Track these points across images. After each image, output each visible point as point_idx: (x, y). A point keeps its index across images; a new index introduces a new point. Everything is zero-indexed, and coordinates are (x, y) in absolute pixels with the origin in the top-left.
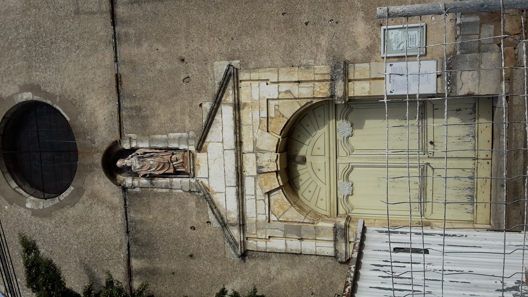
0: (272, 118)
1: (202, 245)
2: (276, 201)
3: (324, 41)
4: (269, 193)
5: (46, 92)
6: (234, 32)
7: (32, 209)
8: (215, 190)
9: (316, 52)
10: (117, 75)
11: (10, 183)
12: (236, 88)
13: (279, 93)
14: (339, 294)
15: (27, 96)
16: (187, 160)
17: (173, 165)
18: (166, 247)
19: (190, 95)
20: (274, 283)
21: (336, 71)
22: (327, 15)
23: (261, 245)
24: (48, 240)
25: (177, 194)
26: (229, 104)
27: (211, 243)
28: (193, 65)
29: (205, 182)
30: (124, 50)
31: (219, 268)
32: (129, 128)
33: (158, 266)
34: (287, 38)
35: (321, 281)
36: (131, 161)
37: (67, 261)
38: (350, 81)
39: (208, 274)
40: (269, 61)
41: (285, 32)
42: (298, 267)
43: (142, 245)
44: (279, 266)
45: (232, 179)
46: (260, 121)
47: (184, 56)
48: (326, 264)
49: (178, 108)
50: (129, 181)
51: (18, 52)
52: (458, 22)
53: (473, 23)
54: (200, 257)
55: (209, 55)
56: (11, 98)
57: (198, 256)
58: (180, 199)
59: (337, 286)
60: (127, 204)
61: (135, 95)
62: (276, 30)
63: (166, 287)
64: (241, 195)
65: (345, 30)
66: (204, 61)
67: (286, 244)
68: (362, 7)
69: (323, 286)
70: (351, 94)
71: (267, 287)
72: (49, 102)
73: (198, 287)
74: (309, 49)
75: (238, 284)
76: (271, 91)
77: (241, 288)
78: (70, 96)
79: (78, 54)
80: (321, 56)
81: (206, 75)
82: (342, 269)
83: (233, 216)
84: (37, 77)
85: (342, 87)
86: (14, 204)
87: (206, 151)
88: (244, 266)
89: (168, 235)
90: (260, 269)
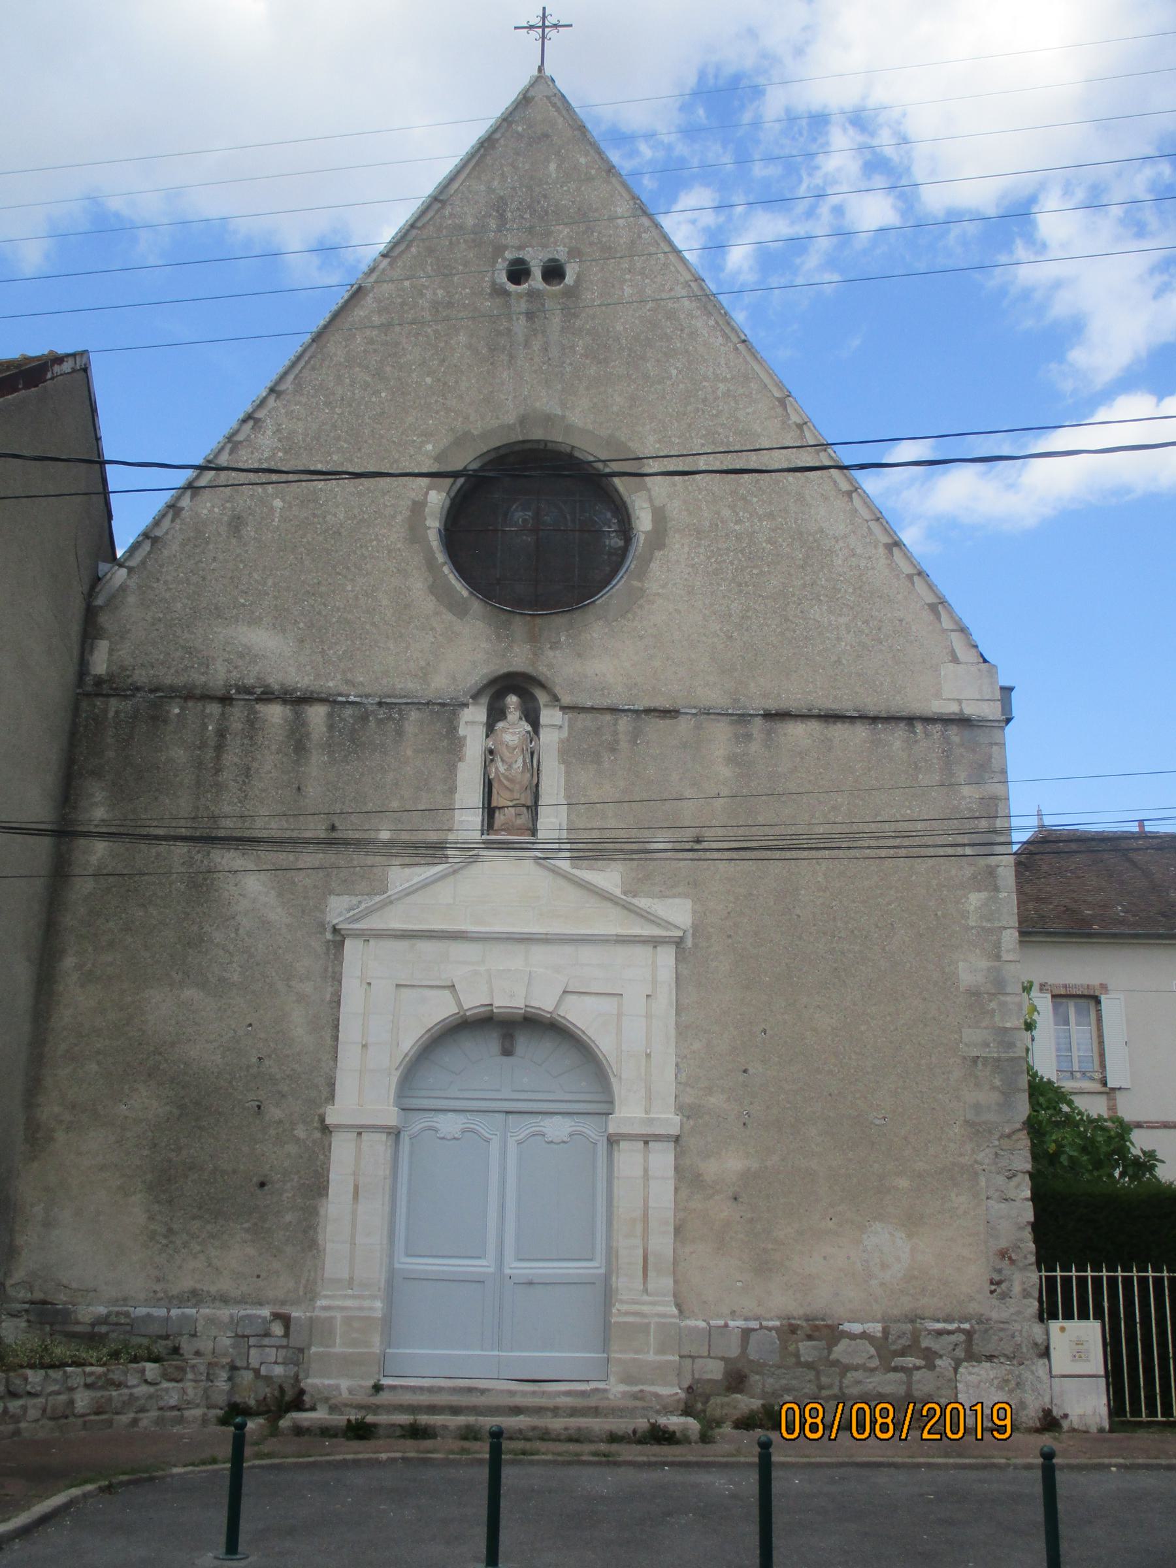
5: (650, 561)
10: (677, 712)
71: (274, 974)
75: (277, 917)
79: (718, 636)
84: (678, 547)
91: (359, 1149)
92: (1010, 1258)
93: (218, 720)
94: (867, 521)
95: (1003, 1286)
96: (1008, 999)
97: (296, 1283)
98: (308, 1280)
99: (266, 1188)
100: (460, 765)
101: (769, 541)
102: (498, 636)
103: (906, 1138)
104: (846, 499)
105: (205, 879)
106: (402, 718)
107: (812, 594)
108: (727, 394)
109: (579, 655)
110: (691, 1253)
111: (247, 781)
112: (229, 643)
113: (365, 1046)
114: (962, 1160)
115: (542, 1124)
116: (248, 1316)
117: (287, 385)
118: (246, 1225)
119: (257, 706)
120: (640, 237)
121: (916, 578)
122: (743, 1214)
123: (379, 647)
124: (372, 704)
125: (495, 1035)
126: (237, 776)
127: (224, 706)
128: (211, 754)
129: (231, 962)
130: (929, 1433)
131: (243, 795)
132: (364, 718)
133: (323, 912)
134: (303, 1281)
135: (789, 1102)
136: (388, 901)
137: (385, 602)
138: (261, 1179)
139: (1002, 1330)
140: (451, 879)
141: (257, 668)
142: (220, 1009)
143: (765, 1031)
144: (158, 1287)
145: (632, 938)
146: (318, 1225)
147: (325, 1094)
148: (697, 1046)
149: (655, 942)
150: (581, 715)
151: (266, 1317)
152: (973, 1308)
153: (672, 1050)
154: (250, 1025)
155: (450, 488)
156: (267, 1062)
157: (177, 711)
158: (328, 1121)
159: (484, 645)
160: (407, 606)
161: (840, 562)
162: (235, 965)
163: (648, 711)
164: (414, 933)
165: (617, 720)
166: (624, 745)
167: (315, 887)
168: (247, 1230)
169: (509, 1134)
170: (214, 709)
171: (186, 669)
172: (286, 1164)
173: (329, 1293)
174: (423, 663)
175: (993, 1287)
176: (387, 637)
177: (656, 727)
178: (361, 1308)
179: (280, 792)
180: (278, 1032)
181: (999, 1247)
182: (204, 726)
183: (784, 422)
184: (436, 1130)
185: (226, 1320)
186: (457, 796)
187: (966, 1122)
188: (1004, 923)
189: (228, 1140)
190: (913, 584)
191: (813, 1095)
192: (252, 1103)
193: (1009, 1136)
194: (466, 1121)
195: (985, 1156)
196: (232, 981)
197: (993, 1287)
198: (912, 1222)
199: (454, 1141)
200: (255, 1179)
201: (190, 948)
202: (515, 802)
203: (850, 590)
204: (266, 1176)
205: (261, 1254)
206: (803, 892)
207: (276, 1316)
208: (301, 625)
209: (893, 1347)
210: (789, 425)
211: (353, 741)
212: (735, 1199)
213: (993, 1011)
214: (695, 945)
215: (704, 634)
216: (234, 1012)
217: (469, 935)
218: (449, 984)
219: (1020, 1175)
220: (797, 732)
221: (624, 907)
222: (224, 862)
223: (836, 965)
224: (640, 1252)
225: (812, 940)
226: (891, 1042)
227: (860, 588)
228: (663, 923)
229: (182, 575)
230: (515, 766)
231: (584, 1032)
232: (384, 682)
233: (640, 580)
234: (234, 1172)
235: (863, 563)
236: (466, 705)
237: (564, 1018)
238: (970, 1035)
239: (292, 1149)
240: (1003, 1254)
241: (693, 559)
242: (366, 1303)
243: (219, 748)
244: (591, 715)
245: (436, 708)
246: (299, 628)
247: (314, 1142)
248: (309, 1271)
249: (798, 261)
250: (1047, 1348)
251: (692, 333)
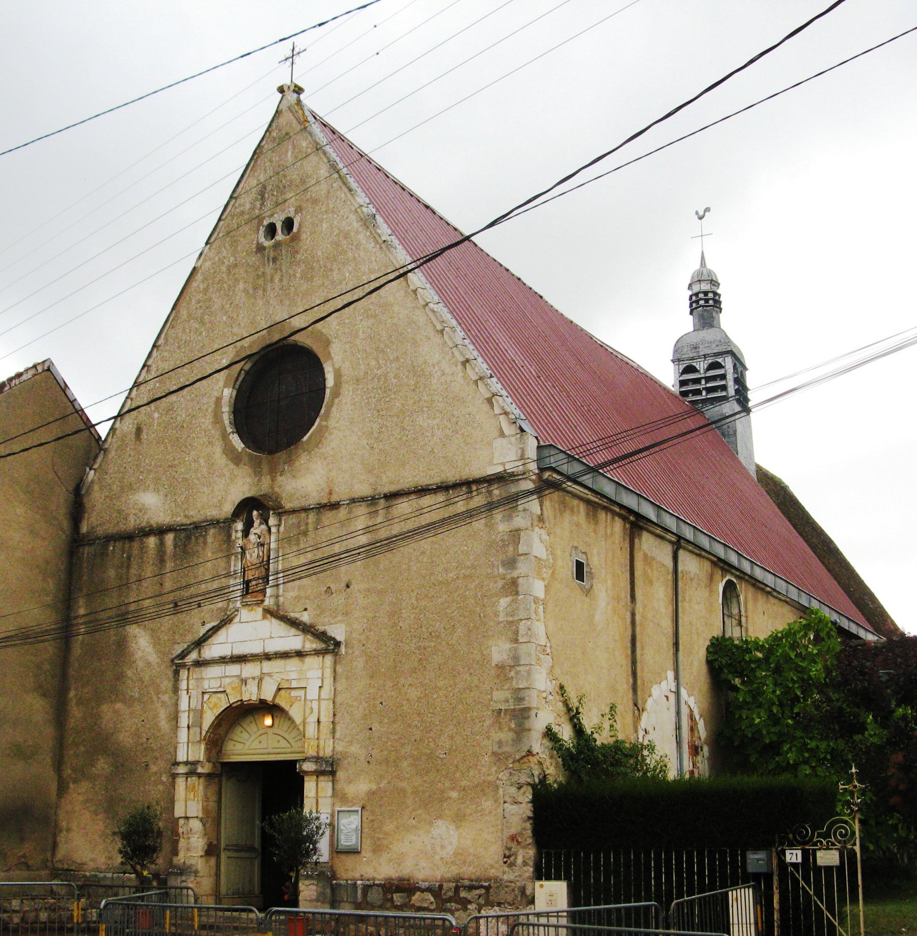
0: (290, 694)
2: (219, 699)
3: (355, 749)
8: (230, 631)
12: (317, 653)
13: (311, 701)
15: (330, 381)
16: (256, 597)
20: (155, 698)
21: (324, 763)
23: (183, 685)
24: (194, 422)
26: (304, 644)
29: (237, 620)
30: (361, 510)
32: (290, 522)
36: (258, 528)
38: (317, 777)
43: (185, 546)
45: (239, 650)
46: (288, 680)
47: (351, 587)
50: (239, 526)
51: (373, 363)
52: (359, 882)
53: (356, 896)
56: (329, 356)
59: (155, 764)
64: (223, 660)
65: (362, 771)
67: (185, 711)
70: (306, 778)
72: (323, 411)
76: (312, 693)
81: (333, 615)
83: (212, 650)
84: (347, 391)
85: (310, 769)
87: (264, 617)
92: (517, 841)
95: (512, 858)
96: (521, 668)
101: (395, 377)
103: (457, 766)
104: (440, 335)
109: (294, 476)
114: (489, 778)
117: (161, 342)
120: (332, 187)
139: (507, 887)
143: (381, 703)
144: (109, 862)
152: (493, 872)
155: (234, 385)
156: (151, 741)
159: (248, 480)
161: (435, 381)
165: (308, 516)
174: (220, 497)
175: (505, 860)
181: (511, 834)
183: (406, 291)
187: (494, 753)
188: (521, 617)
191: (406, 741)
193: (519, 761)
195: (504, 776)
197: (505, 860)
198: (459, 819)
203: (441, 400)
206: (404, 611)
208: (166, 486)
209: (444, 897)
213: (512, 678)
219: (525, 787)
223: (420, 657)
226: (451, 704)
233: (326, 420)
235: (449, 378)
238: (499, 695)
240: (513, 838)
244: (294, 515)
250: (534, 898)
251: (357, 244)
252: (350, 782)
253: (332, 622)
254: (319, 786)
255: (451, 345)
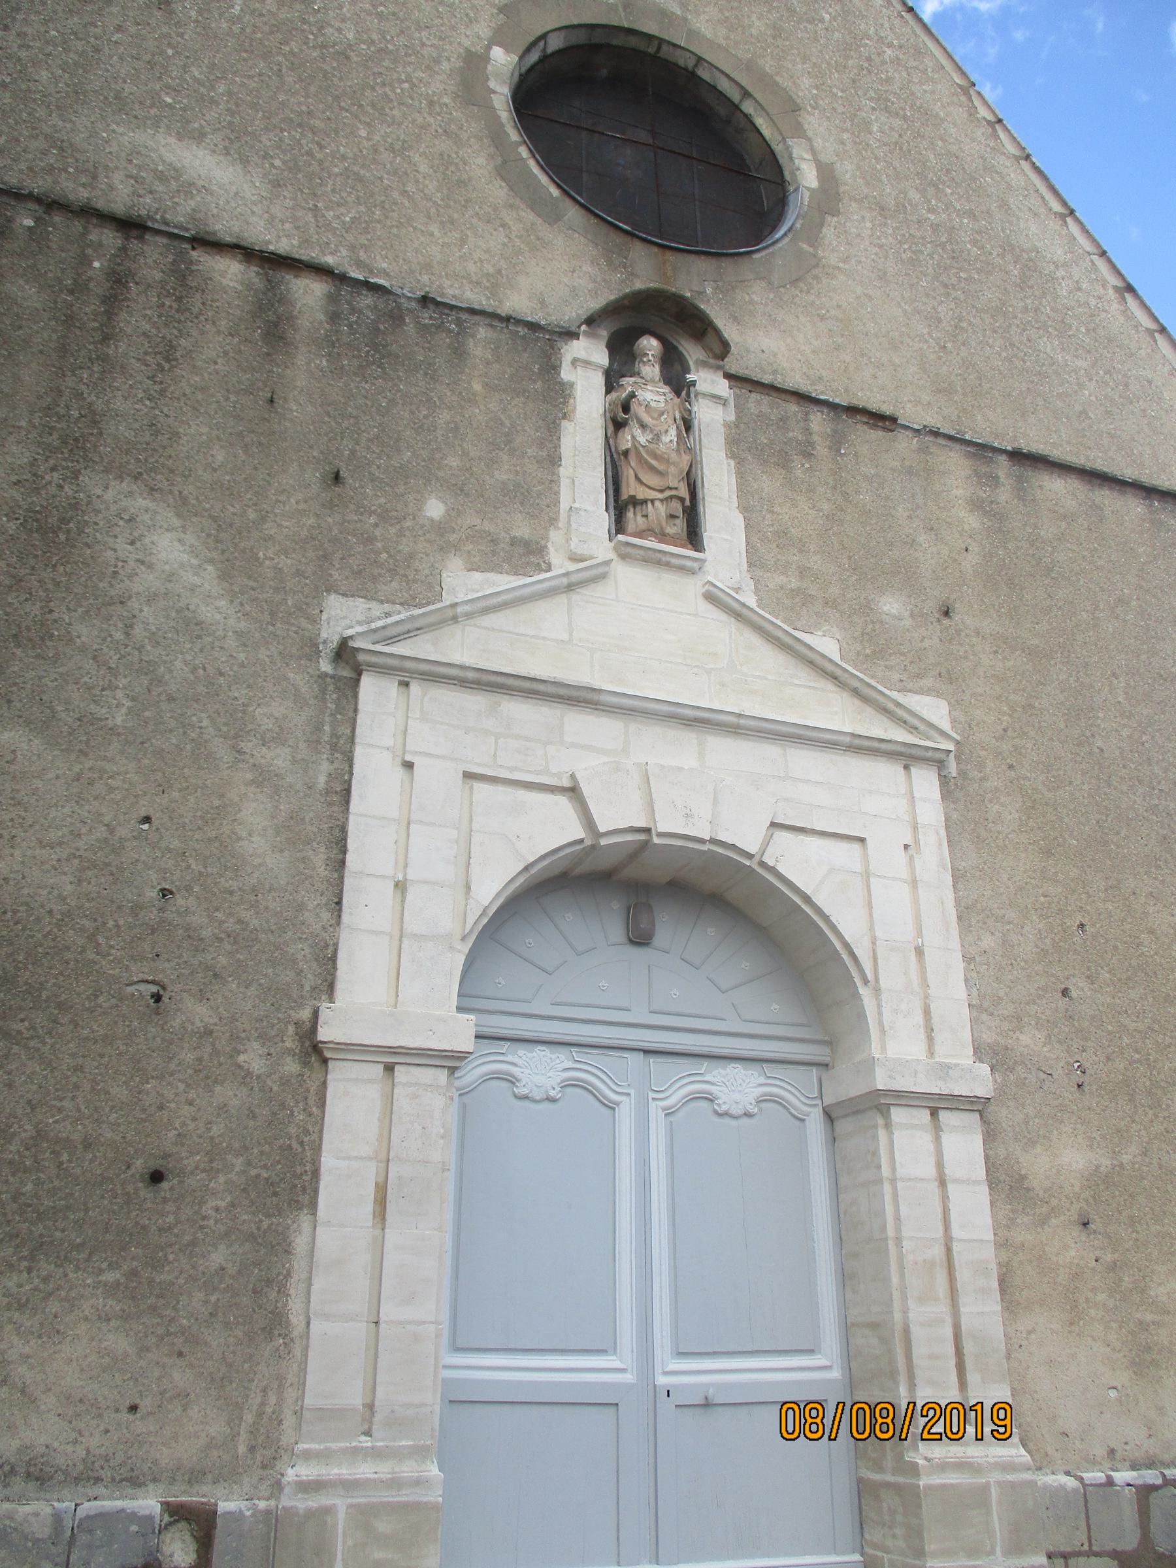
1: (376, 525)
4: (573, 791)
5: (822, 225)
6: (1029, 775)
7: (485, 58)
9: (1000, 1012)
10: (893, 420)
11: (562, 34)
14: (165, 999)
15: (807, 177)
17: (652, 501)
18: (369, 403)
19: (857, 607)
20: (220, 749)
22: (1094, 1058)
25: (556, 488)
27: (384, 556)
28: (936, 640)
31: (284, 562)
33: (301, 360)
34: (1026, 929)
35: (223, 936)
37: (312, 89)
39: (263, 519)
40: (964, 864)
41: (1040, 926)
42: (286, 854)
44: (289, 779)
48: (295, 962)
49: (815, 562)
54: (330, 506)
55: (964, 691)
57: (336, 501)
58: (539, 495)
59: (202, 997)
60: (520, 329)
61: (843, 452)
62: (1042, 899)
63: (216, 363)
66: (948, 672)
68: (1121, 1166)
69: (202, 940)
71: (205, 723)
73: (215, 470)
74: (1006, 994)
75: (218, 616)
77: (202, 623)
78: (818, 283)
79: (926, 342)
80: (989, 1028)
82: (273, 1025)
86: (502, 16)
88: (294, 651)
89: (415, 424)
90: (278, 709)
91: (389, 1101)
93: (114, 256)
94: (1089, 254)
97: (229, 1423)
98: (260, 1414)
99: (165, 1185)
100: (565, 424)
101: (974, 243)
102: (610, 263)
105: (64, 520)
106: (462, 332)
107: (1037, 322)
108: (896, 61)
110: (1030, 1332)
111: (167, 366)
112: (139, 153)
113: (401, 887)
115: (707, 1078)
116: (102, 1516)
118: (110, 1277)
119: (194, 254)
121: (1157, 335)
122: (1098, 1253)
123: (415, 228)
124: (409, 298)
125: (616, 905)
126: (146, 353)
127: (127, 238)
128: (91, 307)
129: (112, 687)
130: (929, 1433)
131: (157, 387)
132: (396, 317)
133: (314, 620)
134: (249, 1418)
135: (1137, 1051)
136: (450, 613)
137: (423, 168)
138: (154, 1164)
140: (562, 599)
141: (192, 203)
142: (78, 777)
145: (876, 745)
146: (288, 1275)
147: (309, 981)
148: (988, 942)
149: (907, 757)
150: (753, 395)
151: (150, 1518)
153: (955, 944)
154: (147, 820)
157: (29, 222)
158: (325, 1034)
160: (461, 183)
162: (119, 694)
163: (853, 410)
164: (500, 680)
166: (821, 450)
167: (298, 573)
168: (112, 1290)
169: (651, 1095)
170: (110, 238)
171: (50, 170)
172: (216, 1130)
173: (315, 1446)
176: (429, 217)
177: (866, 438)
178: (395, 1483)
179: (233, 398)
180: (210, 840)
182: (84, 261)
184: (512, 1080)
185: (42, 1530)
186: (562, 471)
189: (78, 1069)
190: (1155, 341)
192: (142, 987)
194: (570, 1064)
196: (110, 723)
199: (547, 1105)
200: (139, 1163)
201: (18, 645)
202: (668, 493)
204: (166, 1156)
205: (143, 1350)
207: (177, 1513)
210: (978, 119)
211: (375, 346)
212: (1085, 1224)
214: (962, 774)
215: (908, 336)
216: (111, 789)
217: (603, 698)
218: (566, 783)
220: (1055, 486)
221: (855, 692)
222: (109, 495)
224: (948, 1331)
225: (1125, 788)
227: (1094, 330)
228: (922, 727)
229: (53, 33)
230: (666, 439)
231: (807, 899)
232: (425, 278)
234: (87, 1145)
236: (571, 335)
237: (773, 870)
239: (230, 1094)
241: (879, 238)
242: (408, 1469)
243: (113, 301)
245: (522, 331)
246: (272, 165)
247: (285, 1082)
248: (264, 1390)
249: (604, 333)
252: (1033, 1143)
253: (910, 686)
254: (932, 1160)
255: (94, 578)
